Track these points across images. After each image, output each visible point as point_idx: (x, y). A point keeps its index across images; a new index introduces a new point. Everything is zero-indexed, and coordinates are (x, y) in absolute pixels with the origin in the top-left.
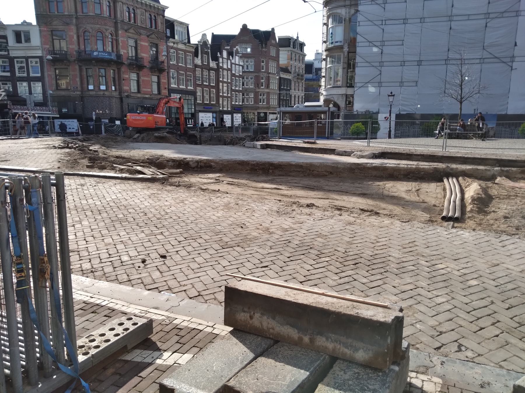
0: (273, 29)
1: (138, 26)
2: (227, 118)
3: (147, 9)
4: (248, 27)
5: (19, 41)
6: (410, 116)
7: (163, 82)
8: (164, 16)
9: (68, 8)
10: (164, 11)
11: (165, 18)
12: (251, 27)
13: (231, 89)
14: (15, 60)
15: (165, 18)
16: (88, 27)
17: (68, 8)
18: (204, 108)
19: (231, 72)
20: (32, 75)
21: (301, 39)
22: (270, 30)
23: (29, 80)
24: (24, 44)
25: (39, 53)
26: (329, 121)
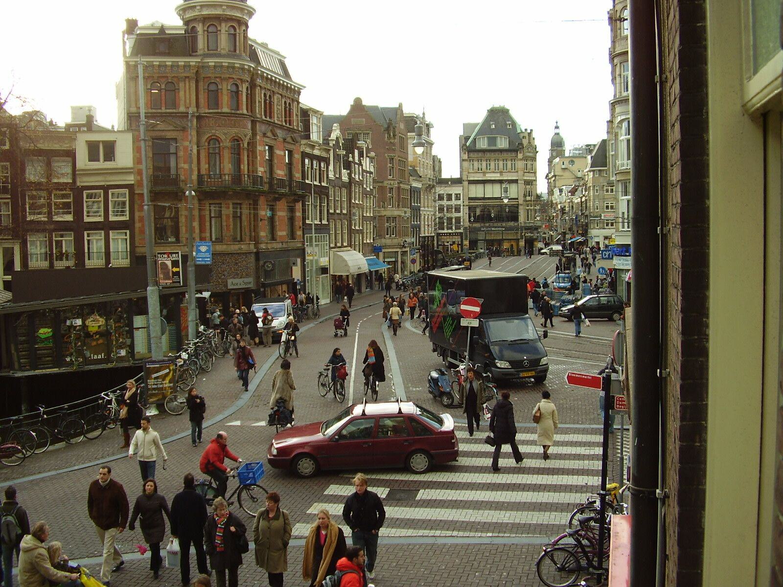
0: (400, 105)
1: (274, 123)
2: (95, 242)
3: (283, 94)
4: (364, 103)
5: (93, 156)
6: (599, 244)
7: (279, 216)
8: (298, 103)
9: (185, 101)
10: (299, 93)
11: (301, 105)
12: (366, 102)
13: (363, 216)
14: (85, 193)
15: (301, 105)
16: (220, 133)
17: (185, 101)
18: (629, 284)
19: (363, 186)
20: (112, 218)
21: (428, 120)
22: (398, 106)
23: (107, 226)
24: (101, 164)
25: (131, 179)
26: (316, 236)
